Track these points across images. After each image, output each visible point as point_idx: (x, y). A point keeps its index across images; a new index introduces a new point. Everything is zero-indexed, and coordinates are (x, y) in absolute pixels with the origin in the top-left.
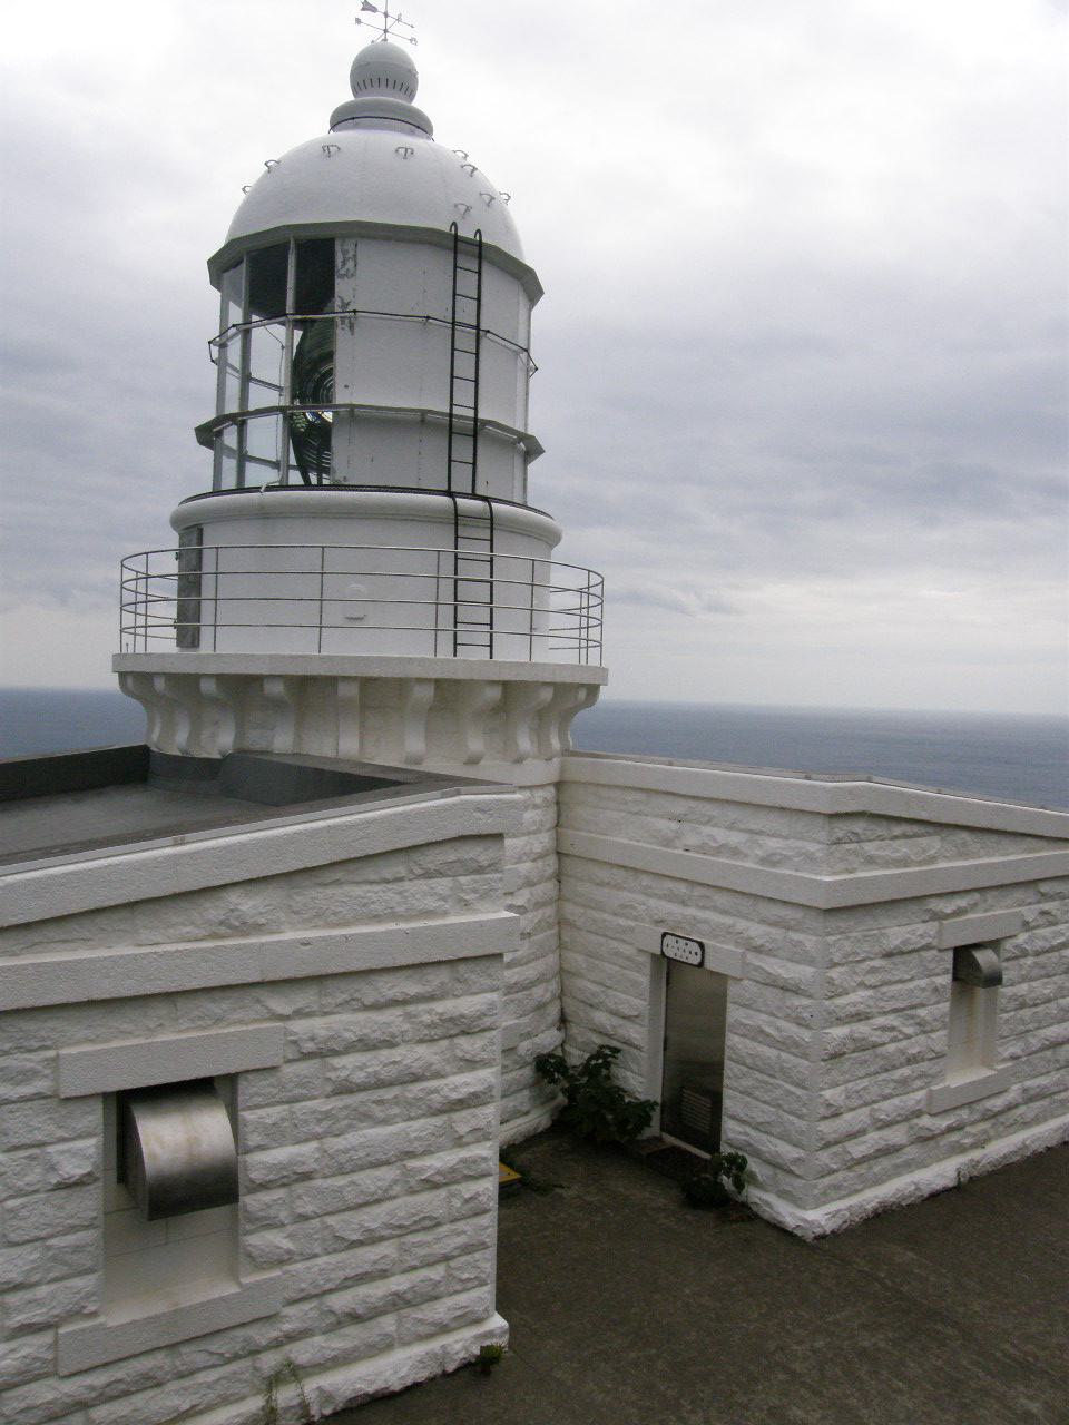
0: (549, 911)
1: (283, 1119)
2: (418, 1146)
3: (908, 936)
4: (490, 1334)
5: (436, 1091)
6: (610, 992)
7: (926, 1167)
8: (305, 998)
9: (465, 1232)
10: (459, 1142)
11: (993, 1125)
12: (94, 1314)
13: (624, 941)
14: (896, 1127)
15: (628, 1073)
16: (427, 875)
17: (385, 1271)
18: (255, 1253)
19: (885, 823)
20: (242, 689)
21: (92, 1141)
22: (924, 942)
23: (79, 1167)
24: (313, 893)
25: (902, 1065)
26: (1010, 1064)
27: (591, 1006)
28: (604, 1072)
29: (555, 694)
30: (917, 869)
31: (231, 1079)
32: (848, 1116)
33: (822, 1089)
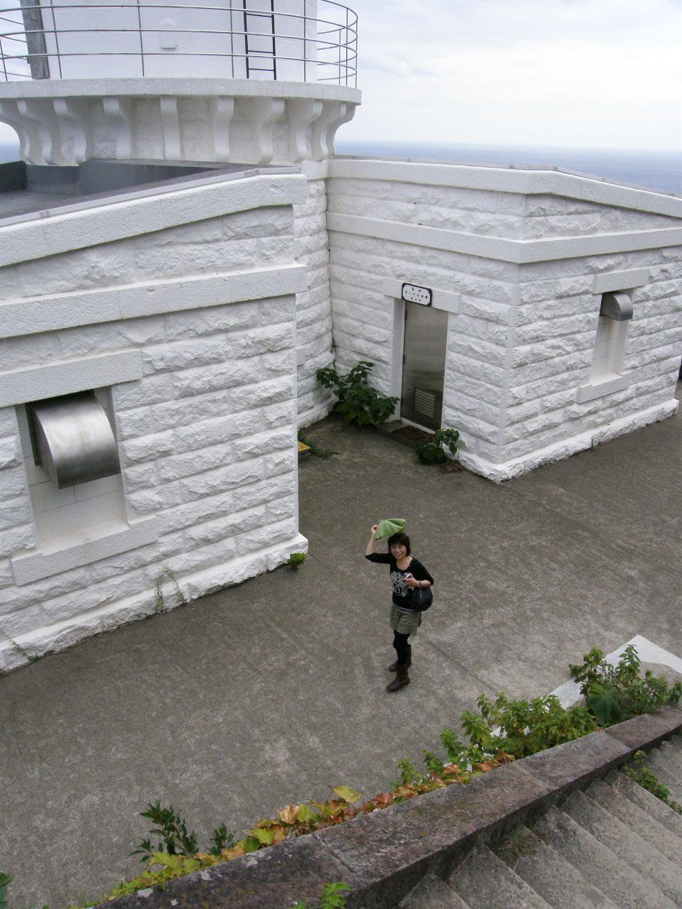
0: (323, 271)
1: (146, 416)
2: (242, 430)
3: (573, 284)
4: (297, 546)
5: (252, 392)
6: (366, 326)
7: (572, 436)
8: (155, 330)
9: (276, 485)
10: (270, 426)
11: (616, 411)
12: (33, 549)
13: (375, 290)
14: (555, 412)
15: (379, 380)
16: (238, 237)
17: (225, 512)
18: (136, 505)
19: (564, 202)
20: (87, 109)
21: (12, 439)
22: (583, 289)
23: (5, 456)
24: (154, 252)
25: (563, 372)
26: (629, 372)
27: (353, 335)
28: (363, 379)
29: (323, 108)
30: (584, 237)
31: (107, 390)
32: (526, 405)
33: (511, 387)
